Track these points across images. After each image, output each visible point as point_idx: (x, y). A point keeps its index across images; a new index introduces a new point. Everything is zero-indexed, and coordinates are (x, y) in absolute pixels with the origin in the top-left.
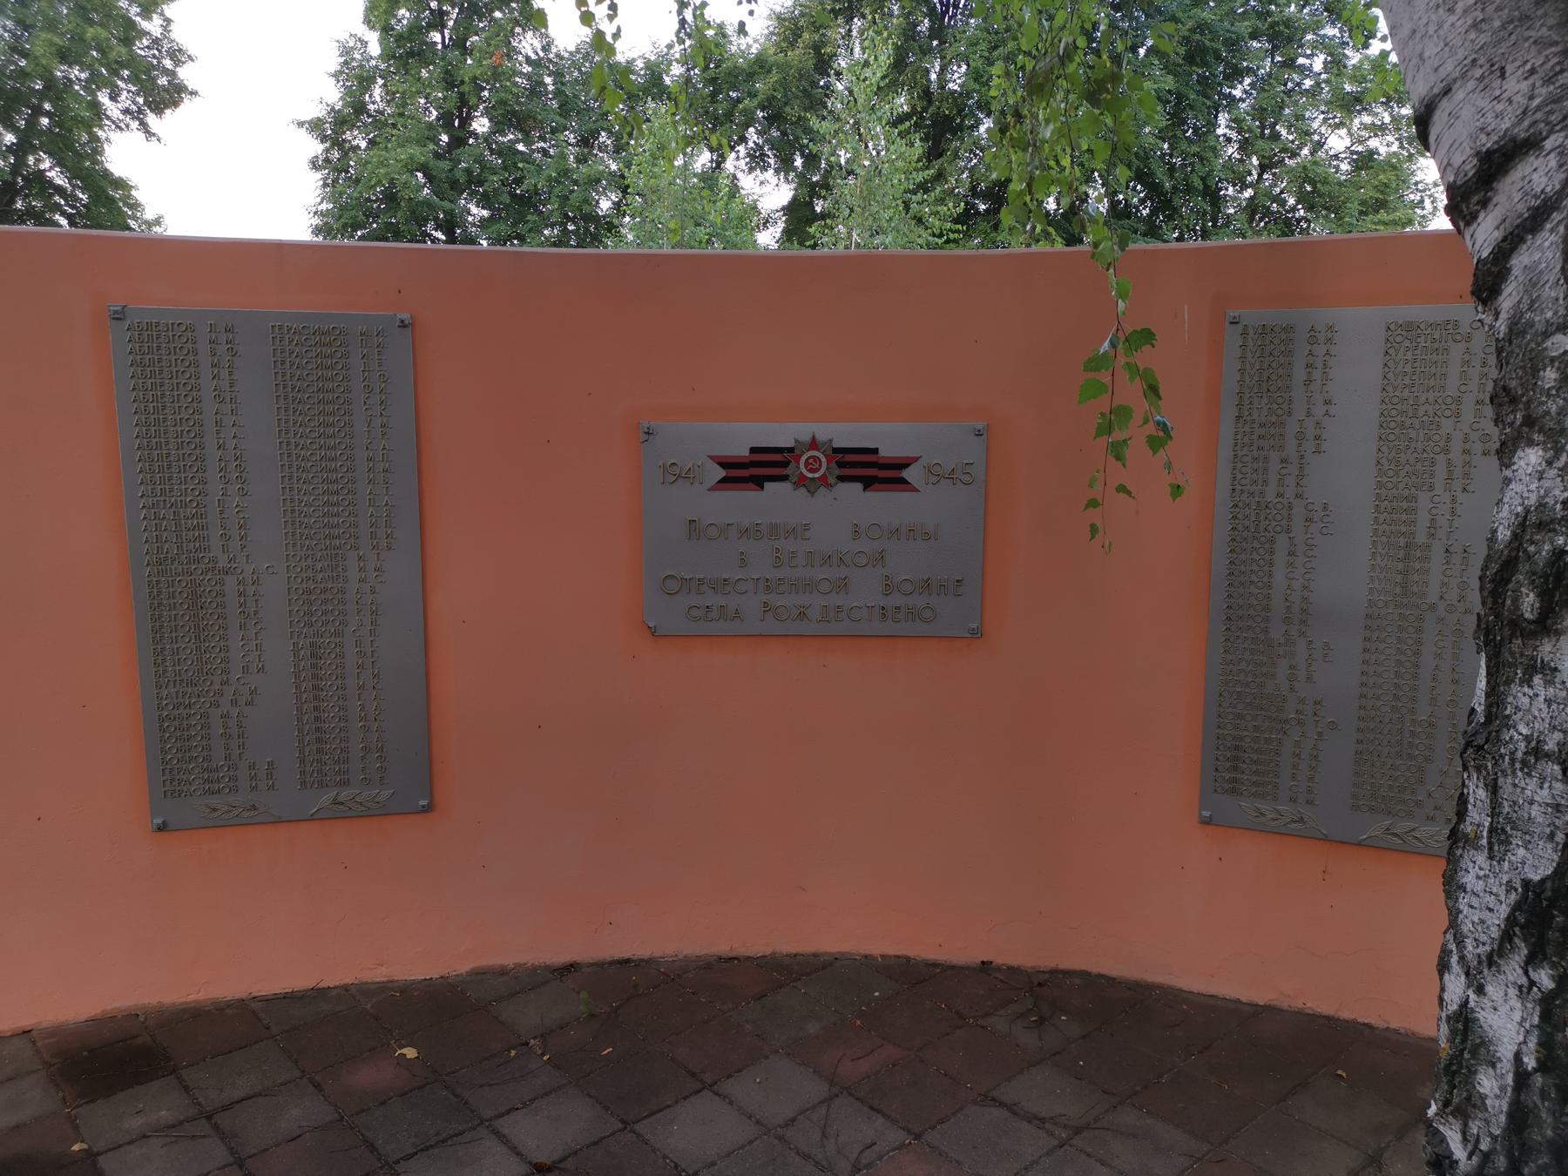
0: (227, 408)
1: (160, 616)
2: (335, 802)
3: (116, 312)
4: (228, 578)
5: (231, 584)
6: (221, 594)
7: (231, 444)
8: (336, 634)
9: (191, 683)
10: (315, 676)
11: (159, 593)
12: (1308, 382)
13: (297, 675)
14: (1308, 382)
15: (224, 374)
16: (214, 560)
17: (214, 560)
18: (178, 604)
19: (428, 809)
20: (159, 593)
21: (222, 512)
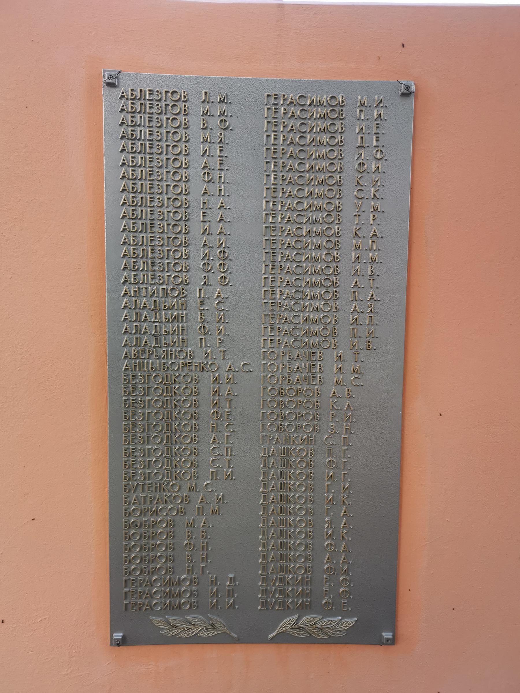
0: (214, 189)
1: (134, 414)
2: (296, 627)
3: (110, 77)
4: (203, 376)
5: (206, 378)
6: (195, 392)
7: (216, 228)
8: (308, 441)
9: (160, 488)
10: (283, 487)
11: (135, 388)
12: (290, 624)
13: (265, 459)
14: (290, 624)
15: (216, 150)
16: (190, 355)
17: (190, 355)
18: (150, 400)
19: (391, 642)
20: (135, 388)
21: (202, 303)
